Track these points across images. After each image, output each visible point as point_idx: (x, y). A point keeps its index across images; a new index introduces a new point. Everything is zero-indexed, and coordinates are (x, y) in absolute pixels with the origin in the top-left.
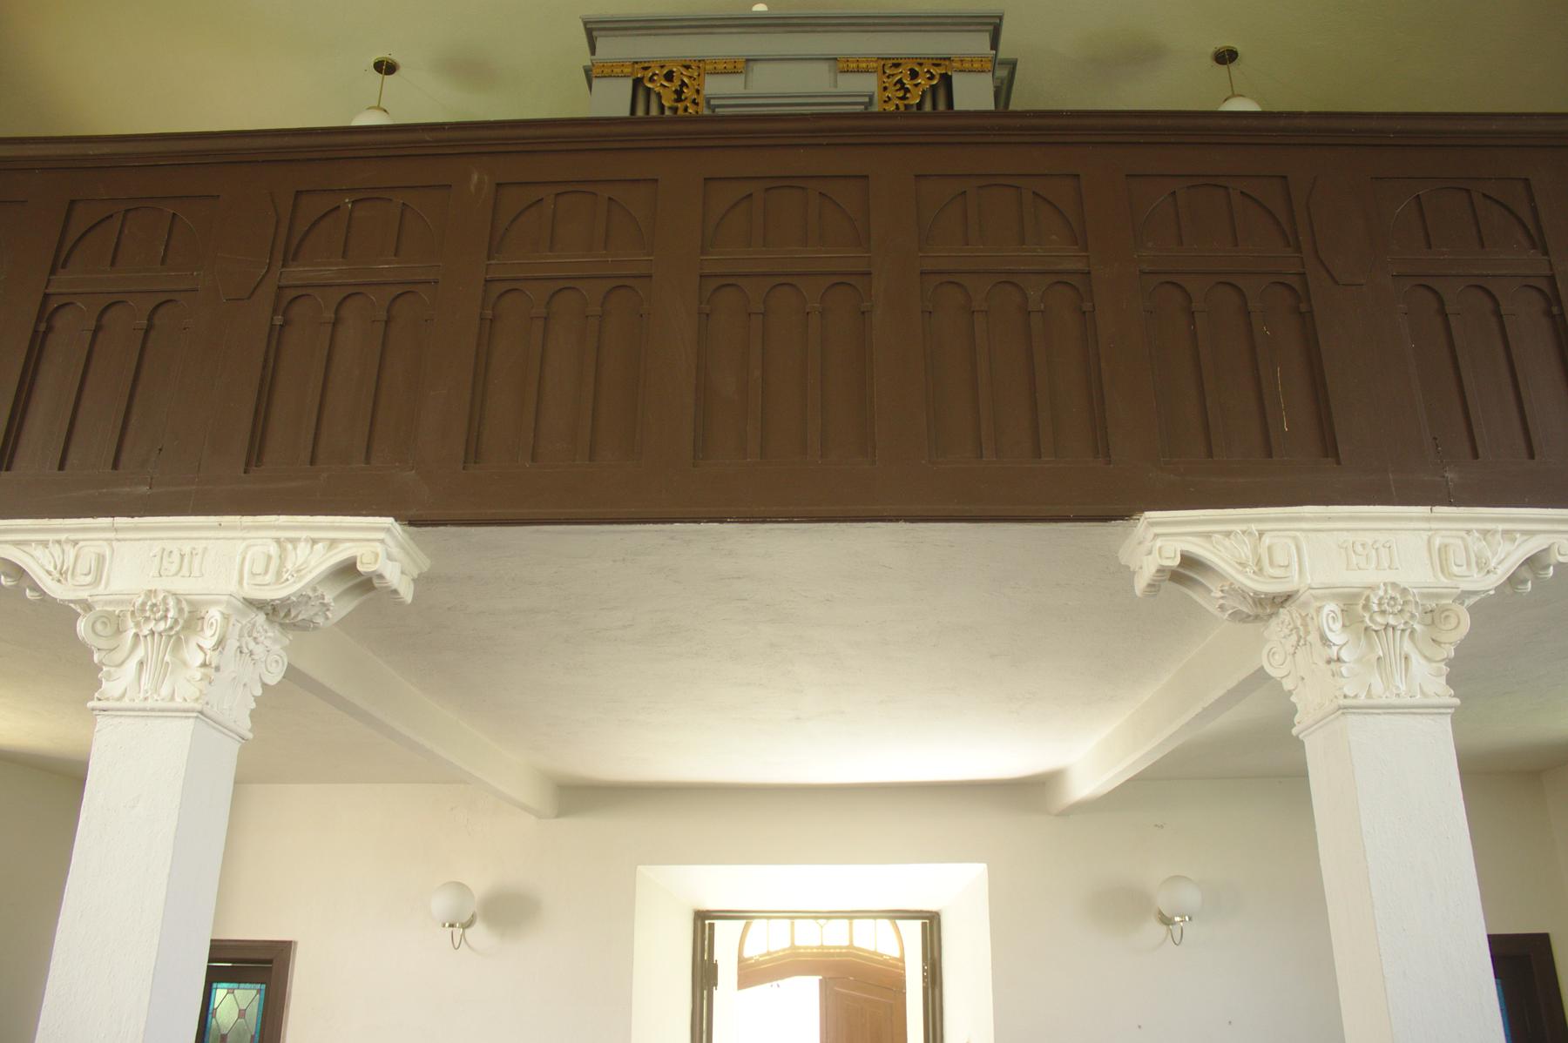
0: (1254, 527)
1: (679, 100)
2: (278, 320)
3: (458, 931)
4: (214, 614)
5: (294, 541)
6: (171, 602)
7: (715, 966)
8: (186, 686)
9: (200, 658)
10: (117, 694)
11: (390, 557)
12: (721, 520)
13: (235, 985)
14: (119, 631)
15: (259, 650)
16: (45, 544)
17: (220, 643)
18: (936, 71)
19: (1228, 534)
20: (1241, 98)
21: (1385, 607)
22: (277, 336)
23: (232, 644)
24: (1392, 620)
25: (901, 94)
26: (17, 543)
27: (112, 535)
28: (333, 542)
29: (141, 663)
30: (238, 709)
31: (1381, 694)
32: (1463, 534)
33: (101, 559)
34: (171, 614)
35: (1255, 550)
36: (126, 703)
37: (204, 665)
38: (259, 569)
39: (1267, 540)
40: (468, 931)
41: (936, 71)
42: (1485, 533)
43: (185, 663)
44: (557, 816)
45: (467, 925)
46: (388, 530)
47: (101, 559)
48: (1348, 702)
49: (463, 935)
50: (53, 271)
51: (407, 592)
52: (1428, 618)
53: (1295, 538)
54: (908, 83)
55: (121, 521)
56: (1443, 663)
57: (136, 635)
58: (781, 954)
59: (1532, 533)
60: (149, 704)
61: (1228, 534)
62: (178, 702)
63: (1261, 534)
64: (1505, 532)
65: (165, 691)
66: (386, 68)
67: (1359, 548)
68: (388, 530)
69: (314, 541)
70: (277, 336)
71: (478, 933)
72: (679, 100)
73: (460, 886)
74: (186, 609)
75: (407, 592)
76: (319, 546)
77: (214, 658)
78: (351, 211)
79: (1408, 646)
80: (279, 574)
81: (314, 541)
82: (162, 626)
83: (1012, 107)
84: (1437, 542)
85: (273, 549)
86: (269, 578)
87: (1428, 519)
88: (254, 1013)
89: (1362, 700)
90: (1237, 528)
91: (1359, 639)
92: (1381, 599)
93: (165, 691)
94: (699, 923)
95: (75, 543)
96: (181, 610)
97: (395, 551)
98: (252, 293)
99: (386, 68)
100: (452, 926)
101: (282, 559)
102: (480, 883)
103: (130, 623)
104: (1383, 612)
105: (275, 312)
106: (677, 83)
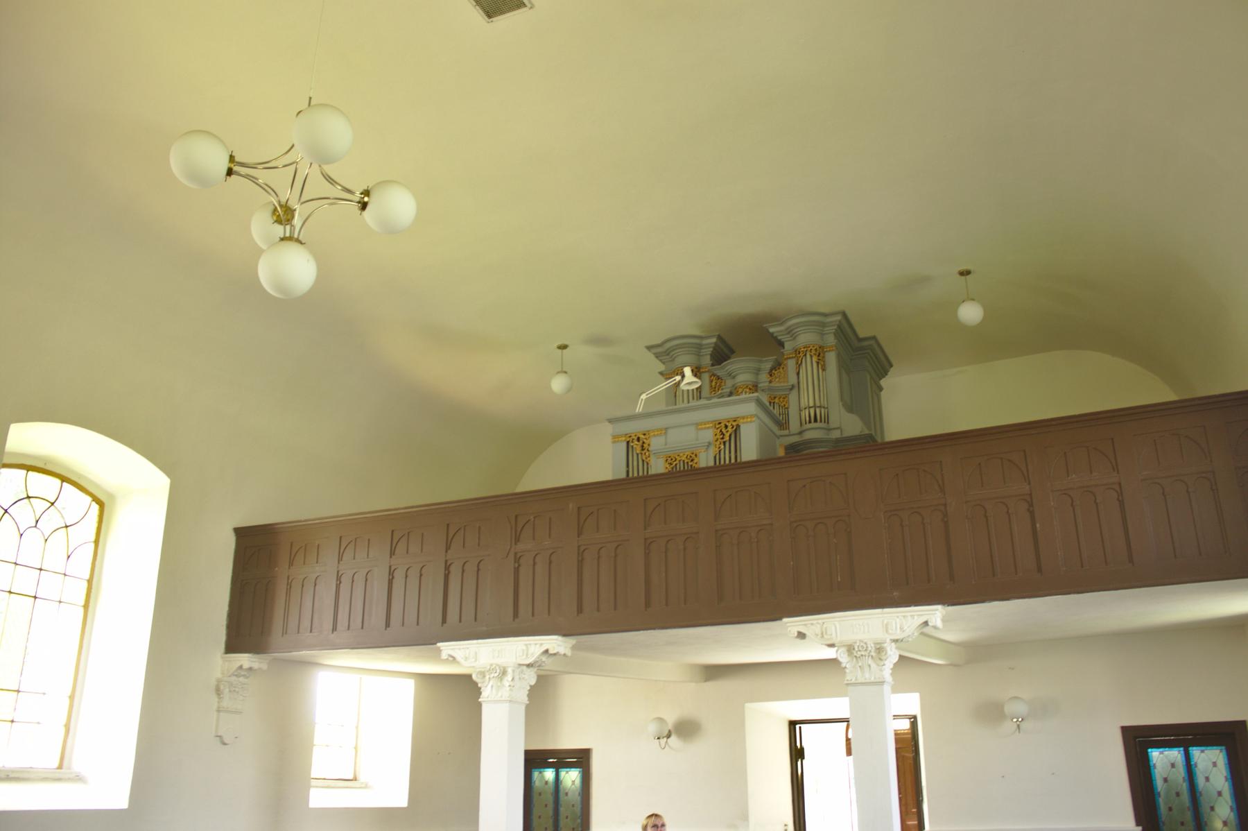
0: (820, 621)
1: (643, 450)
2: (517, 565)
3: (663, 741)
4: (510, 670)
5: (530, 644)
6: (497, 668)
7: (803, 749)
8: (505, 693)
9: (508, 684)
10: (486, 696)
11: (559, 645)
12: (654, 629)
13: (568, 770)
14: (484, 677)
15: (526, 677)
16: (460, 649)
17: (513, 679)
18: (734, 424)
19: (812, 624)
20: (973, 302)
21: (861, 649)
22: (517, 571)
23: (517, 677)
24: (863, 653)
25: (721, 436)
26: (452, 649)
27: (478, 645)
28: (541, 644)
29: (492, 686)
30: (523, 697)
31: (861, 680)
32: (896, 618)
33: (476, 653)
34: (498, 671)
35: (822, 629)
36: (489, 699)
37: (510, 686)
38: (521, 654)
39: (825, 626)
40: (669, 740)
41: (734, 424)
42: (904, 616)
43: (503, 686)
44: (705, 681)
45: (669, 736)
46: (556, 640)
47: (476, 653)
48: (849, 682)
49: (667, 742)
50: (446, 552)
51: (569, 653)
52: (878, 651)
53: (834, 624)
54: (724, 430)
55: (480, 641)
56: (849, 677)
57: (489, 678)
58: (902, 732)
59: (921, 615)
60: (495, 699)
61: (812, 624)
62: (503, 699)
63: (824, 623)
64: (911, 616)
65: (500, 694)
66: (563, 347)
67: (857, 626)
68: (556, 640)
69: (536, 644)
70: (517, 571)
71: (673, 738)
72: (643, 450)
73: (661, 720)
74: (502, 669)
75: (569, 653)
76: (538, 646)
77: (512, 684)
78: (534, 521)
79: (870, 661)
80: (527, 655)
81: (536, 644)
82: (496, 675)
83: (744, 459)
84: (885, 622)
85: (524, 648)
86: (525, 657)
87: (881, 614)
88: (578, 782)
89: (853, 681)
90: (815, 622)
91: (853, 660)
92: (858, 646)
93: (500, 694)
94: (792, 727)
95: (468, 648)
96: (500, 670)
97: (561, 643)
98: (508, 554)
99: (563, 347)
100: (658, 738)
101: (528, 650)
102: (671, 719)
103: (487, 674)
104: (860, 651)
105: (515, 562)
106: (641, 442)
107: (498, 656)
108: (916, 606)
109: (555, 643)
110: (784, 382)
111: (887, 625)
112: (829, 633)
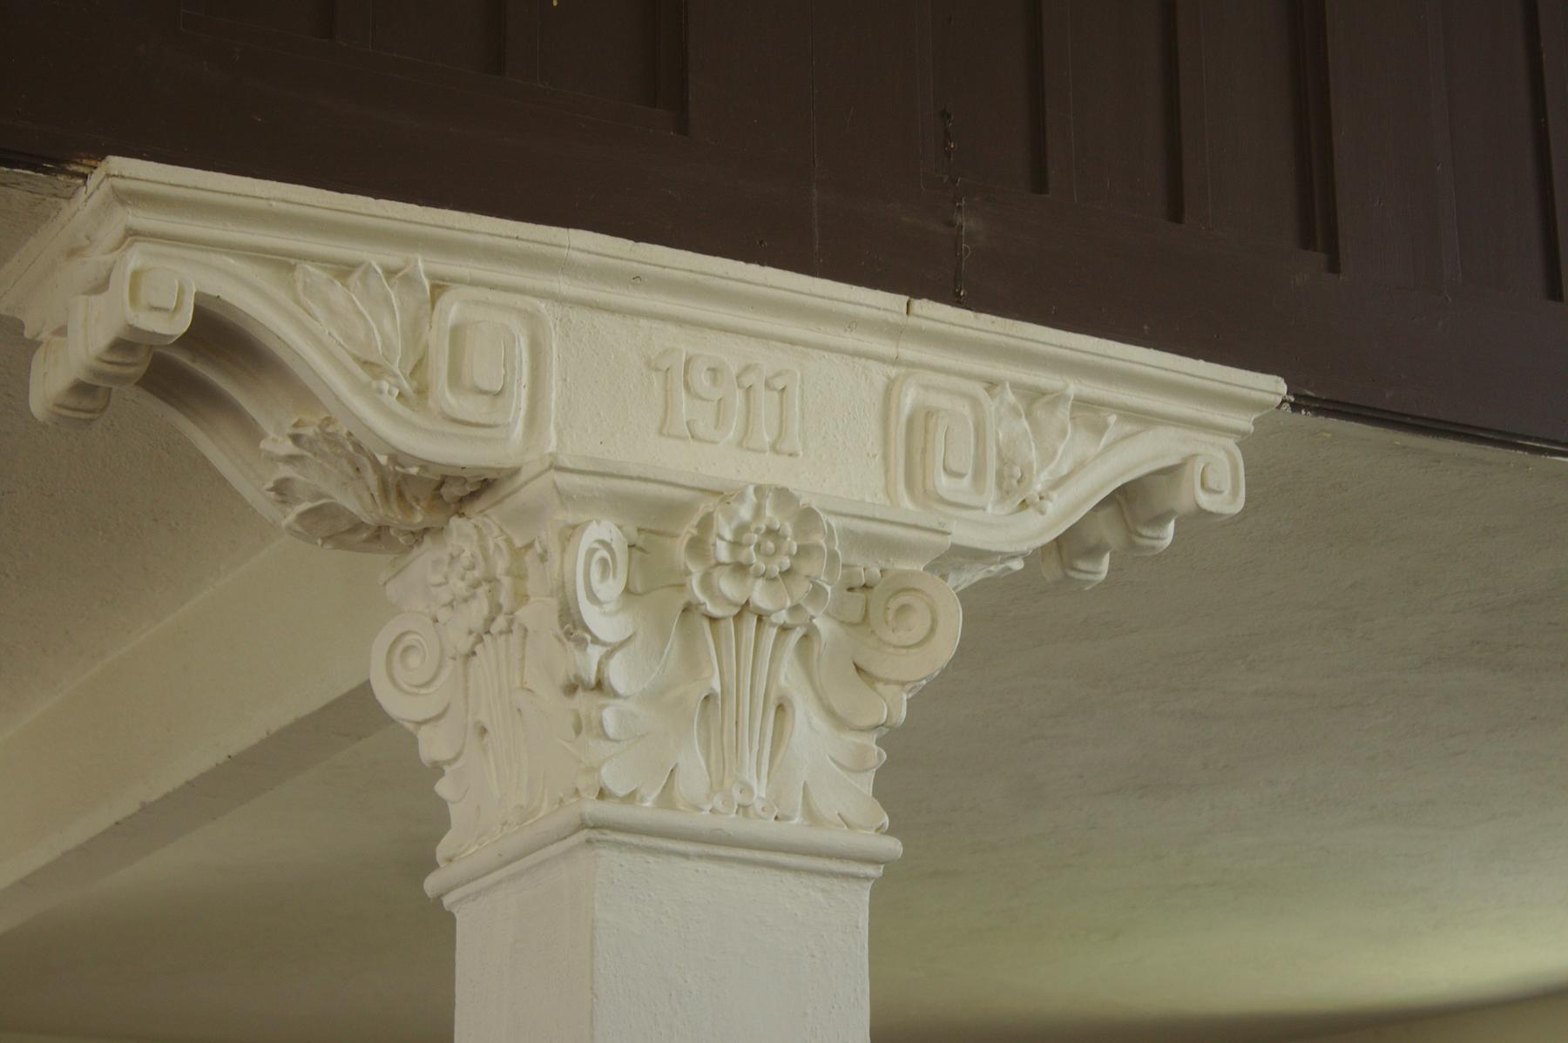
0: (423, 264)
21: (749, 554)
24: (760, 595)
39: (452, 308)
48: (607, 810)
52: (854, 611)
53: (531, 318)
61: (343, 270)
63: (439, 287)
79: (789, 676)
84: (909, 398)
89: (647, 810)
90: (376, 257)
104: (740, 568)
107: (285, 517)
108: (1207, 359)
109: (883, 762)
110: (36, 199)
111: (921, 421)
112: (482, 371)
